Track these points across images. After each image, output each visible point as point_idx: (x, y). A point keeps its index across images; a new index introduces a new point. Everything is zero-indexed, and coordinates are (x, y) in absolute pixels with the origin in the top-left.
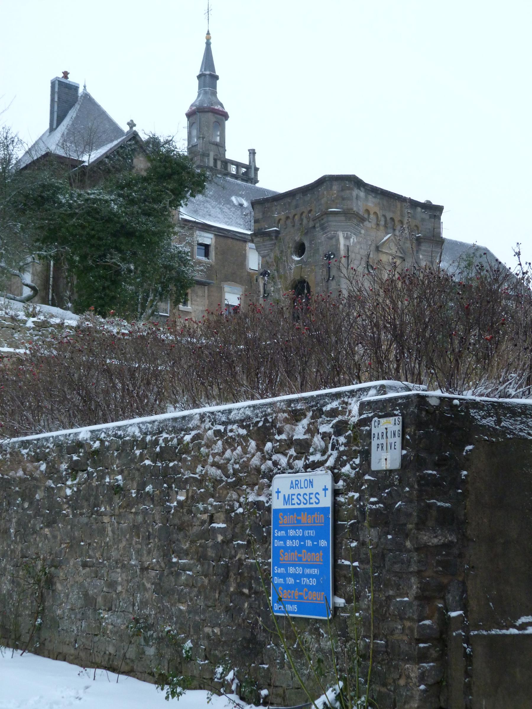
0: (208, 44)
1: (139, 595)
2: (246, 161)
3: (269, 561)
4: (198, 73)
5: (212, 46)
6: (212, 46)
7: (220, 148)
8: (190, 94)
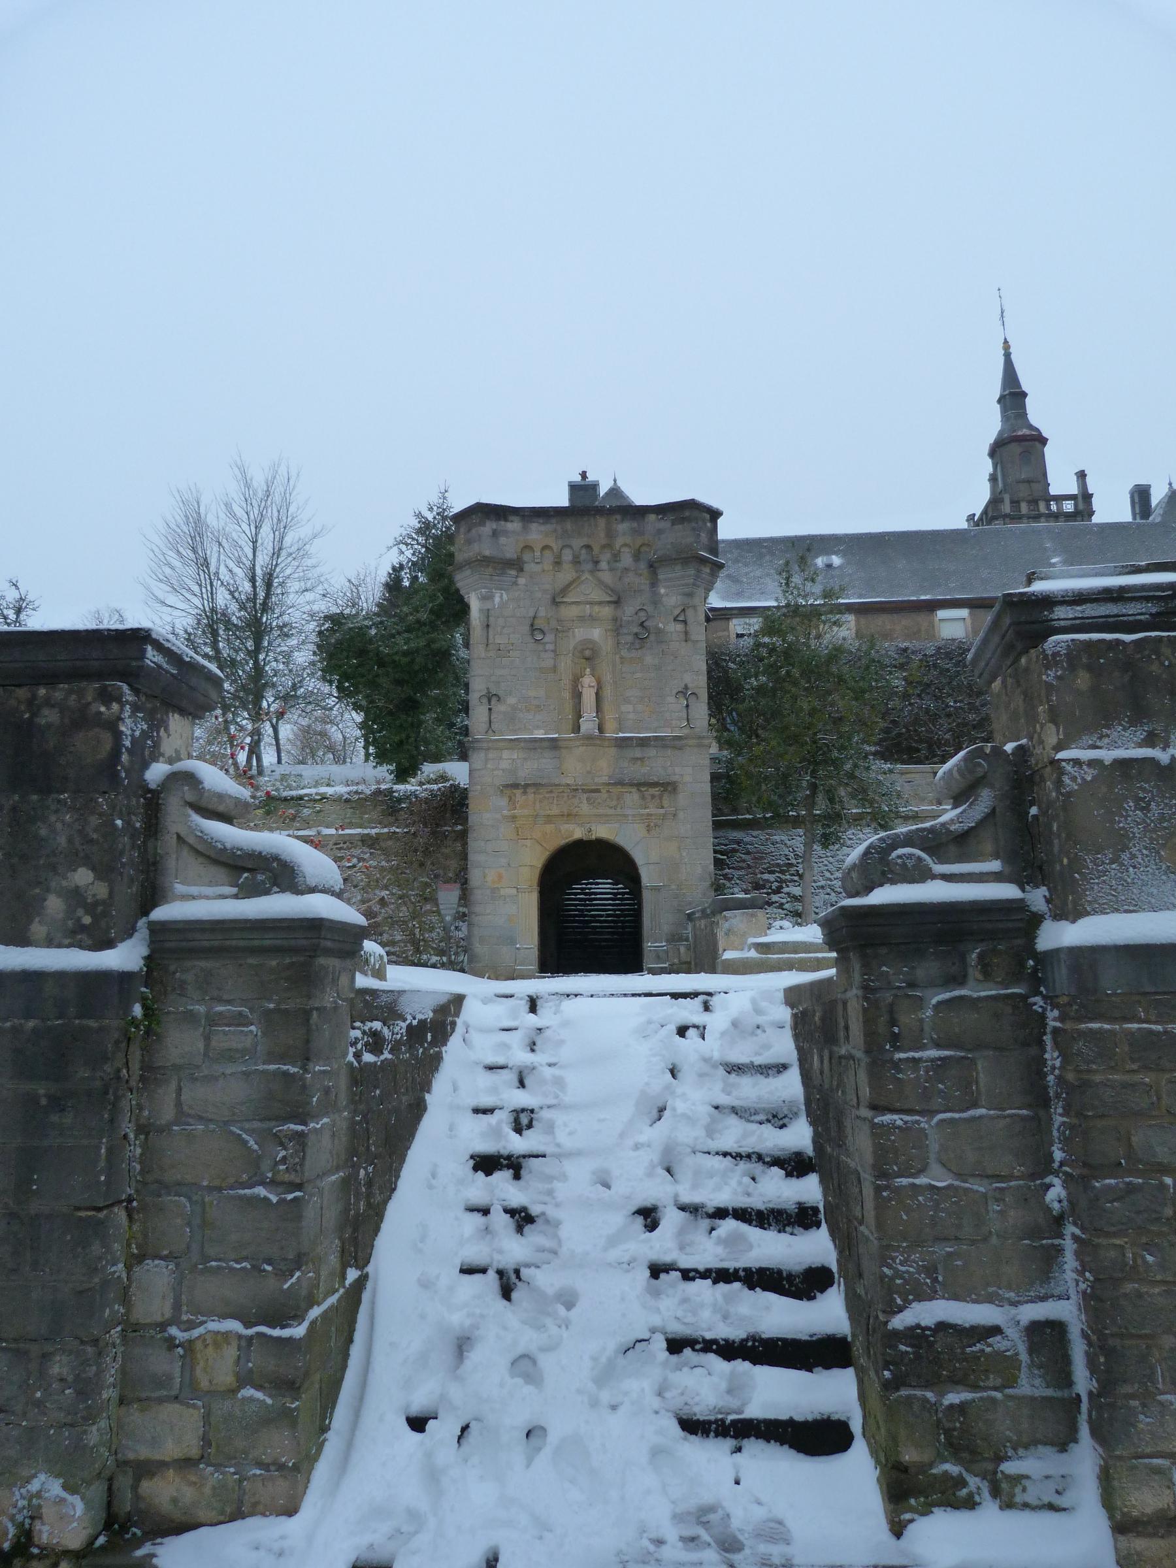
3: (390, 1056)
5: (1012, 356)
6: (1014, 358)
7: (1033, 485)
8: (991, 424)
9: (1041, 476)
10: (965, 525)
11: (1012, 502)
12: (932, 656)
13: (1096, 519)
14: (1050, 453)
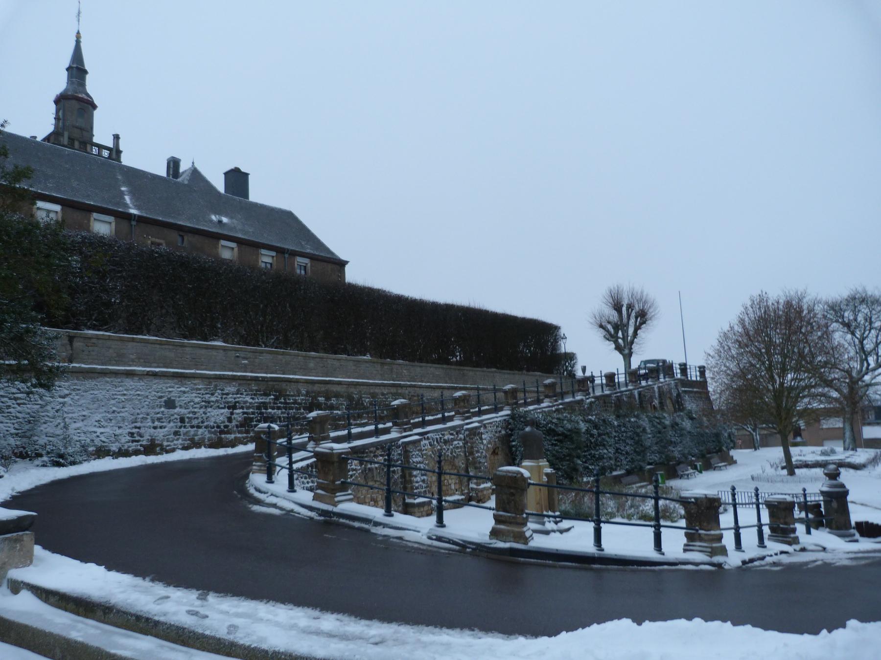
0: (78, 42)
1: (393, 403)
2: (110, 144)
4: (67, 66)
6: (83, 45)
8: (60, 83)
9: (88, 129)
10: (162, 172)
11: (69, 138)
12: (79, 243)
14: (98, 116)
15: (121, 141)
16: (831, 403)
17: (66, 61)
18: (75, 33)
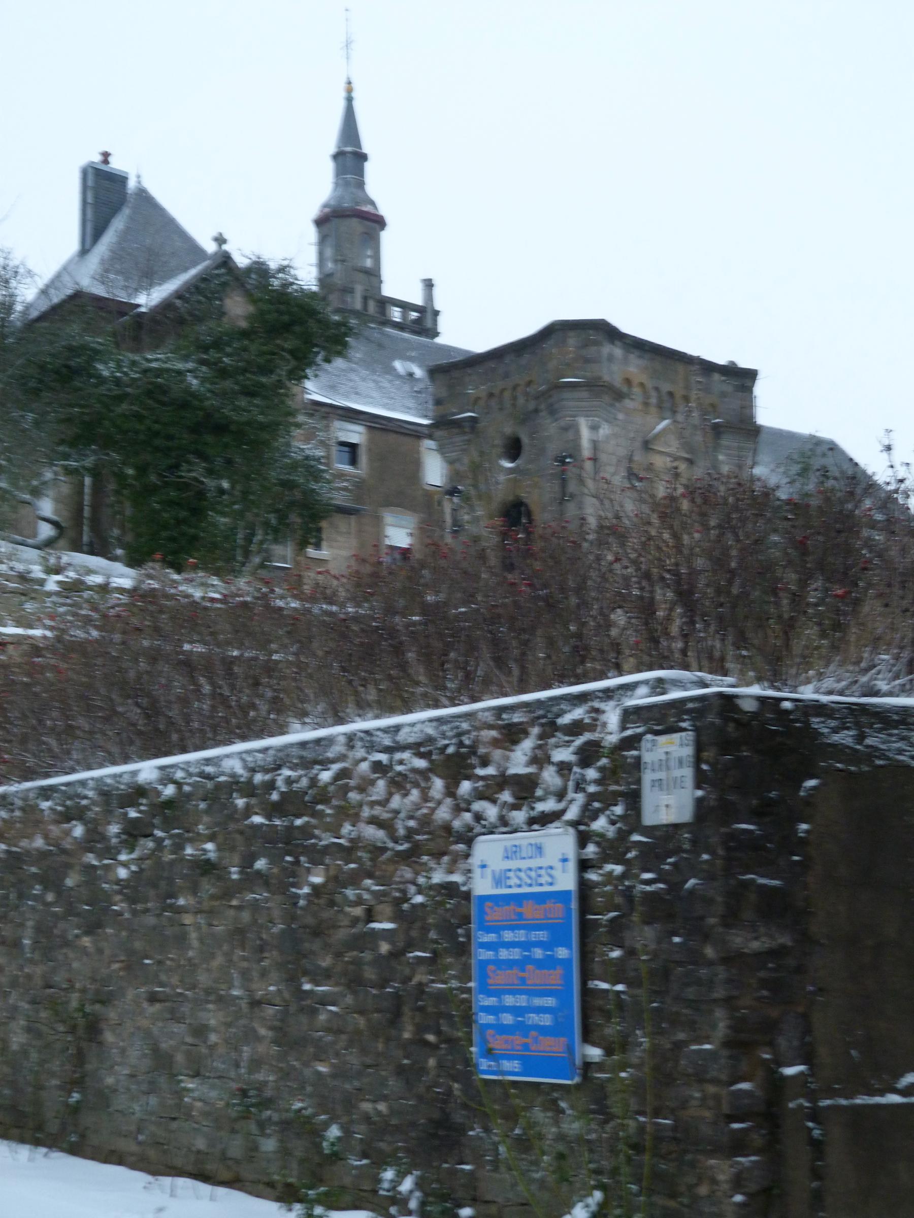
0: (349, 100)
2: (416, 297)
8: (321, 187)
13: (439, 340)
14: (389, 241)
15: (437, 292)
16: (49, 845)
17: (331, 143)
18: (344, 80)
